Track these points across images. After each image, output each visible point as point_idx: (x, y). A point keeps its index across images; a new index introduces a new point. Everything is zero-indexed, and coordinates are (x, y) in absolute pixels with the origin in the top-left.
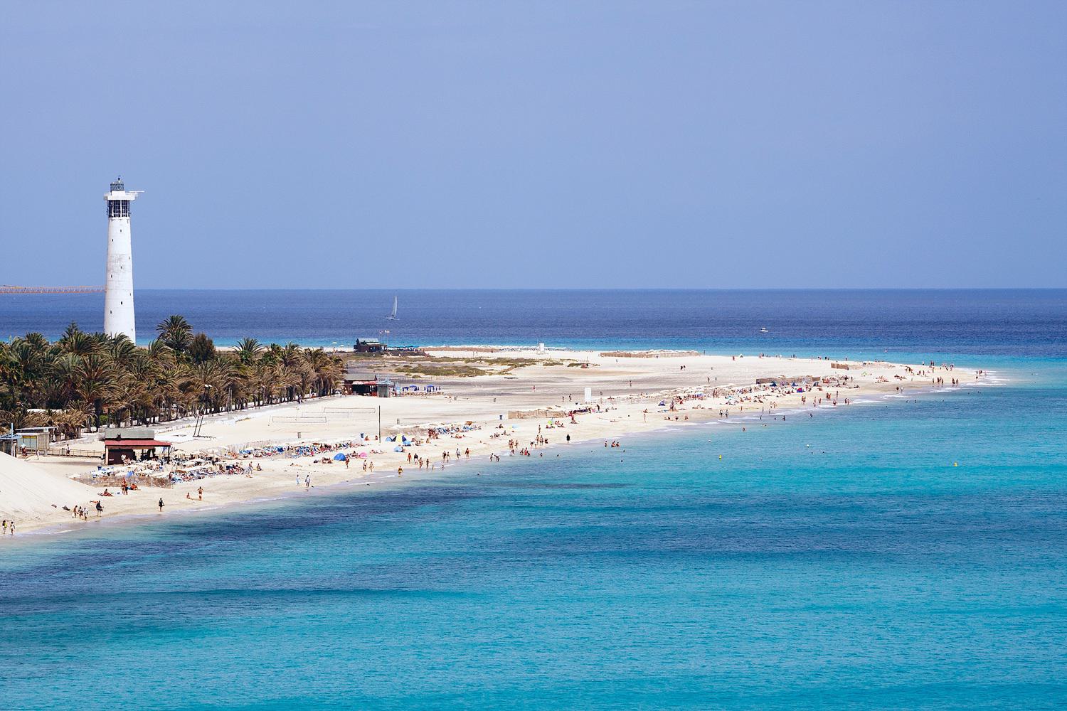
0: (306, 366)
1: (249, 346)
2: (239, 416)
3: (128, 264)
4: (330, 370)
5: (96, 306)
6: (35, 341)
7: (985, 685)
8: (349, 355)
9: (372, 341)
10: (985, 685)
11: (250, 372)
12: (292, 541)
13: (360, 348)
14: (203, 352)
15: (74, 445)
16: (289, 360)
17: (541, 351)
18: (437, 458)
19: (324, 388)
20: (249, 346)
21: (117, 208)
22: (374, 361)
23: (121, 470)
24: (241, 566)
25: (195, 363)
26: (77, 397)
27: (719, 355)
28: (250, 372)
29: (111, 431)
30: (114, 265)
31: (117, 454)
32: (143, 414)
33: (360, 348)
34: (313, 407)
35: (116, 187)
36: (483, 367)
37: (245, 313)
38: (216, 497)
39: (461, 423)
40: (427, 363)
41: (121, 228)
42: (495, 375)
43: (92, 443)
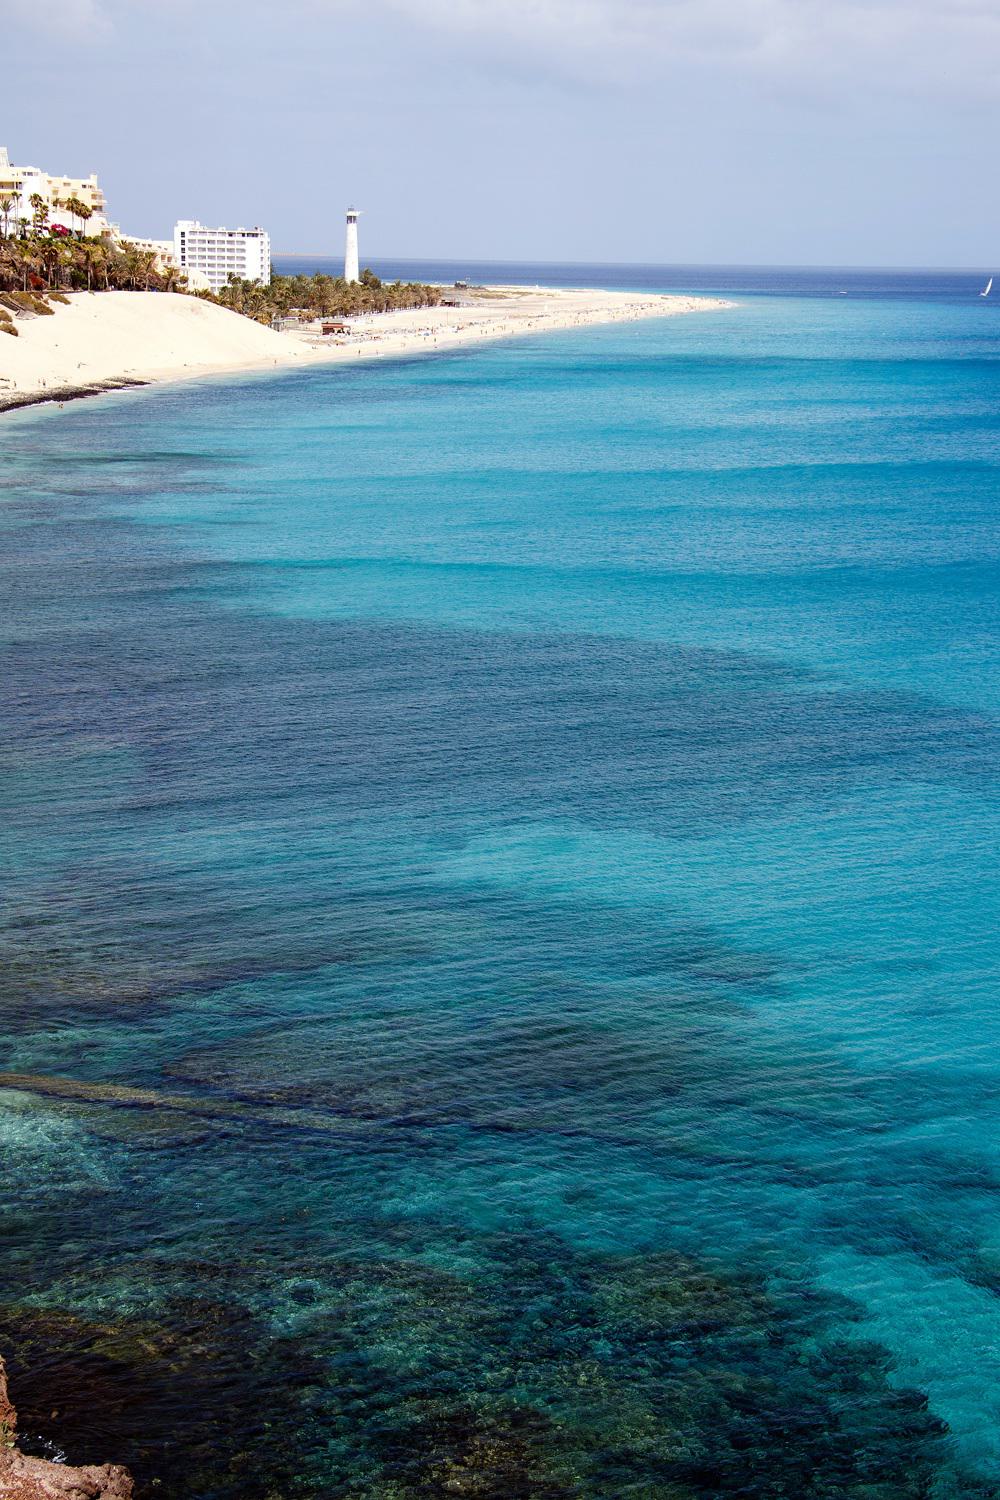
0: (423, 293)
1: (398, 285)
2: (391, 314)
3: (356, 244)
4: (434, 295)
5: (341, 267)
6: (299, 279)
7: (252, 1089)
8: (451, 289)
9: (463, 283)
10: (252, 1089)
11: (396, 295)
13: (457, 285)
14: (376, 285)
15: (310, 326)
16: (415, 290)
17: (536, 289)
19: (431, 303)
20: (398, 285)
21: (350, 219)
25: (379, 291)
27: (628, 291)
28: (396, 295)
29: (325, 320)
30: (349, 245)
31: (327, 330)
32: (345, 312)
33: (457, 285)
34: (425, 313)
35: (351, 210)
36: (510, 295)
38: (371, 350)
40: (485, 293)
41: (352, 228)
42: (512, 301)
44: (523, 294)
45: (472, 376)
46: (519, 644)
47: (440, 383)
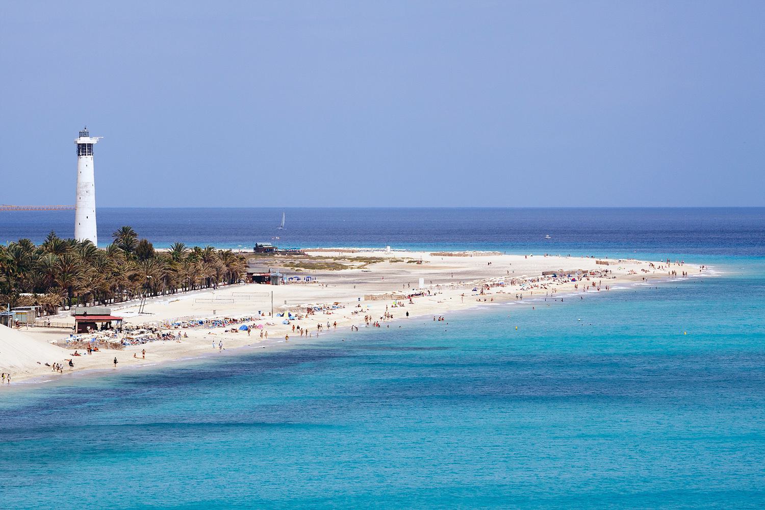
0: (220, 263)
1: (179, 248)
2: (172, 298)
3: (92, 189)
4: (237, 265)
5: (69, 219)
8: (250, 255)
9: (267, 244)
11: (179, 267)
13: (258, 250)
14: (145, 253)
15: (53, 319)
16: (208, 258)
17: (388, 252)
18: (313, 329)
19: (232, 279)
20: (179, 248)
21: (84, 149)
22: (268, 259)
23: (87, 337)
25: (140, 260)
26: (55, 285)
28: (179, 267)
29: (80, 309)
30: (82, 190)
31: (84, 326)
32: (103, 297)
33: (258, 250)
34: (225, 292)
35: (83, 134)
36: (347, 263)
38: (155, 357)
39: (331, 303)
40: (306, 261)
41: (87, 163)
42: (355, 269)
43: (66, 318)
44: (370, 261)
45: (429, 346)
46: (728, 279)
47: (401, 349)
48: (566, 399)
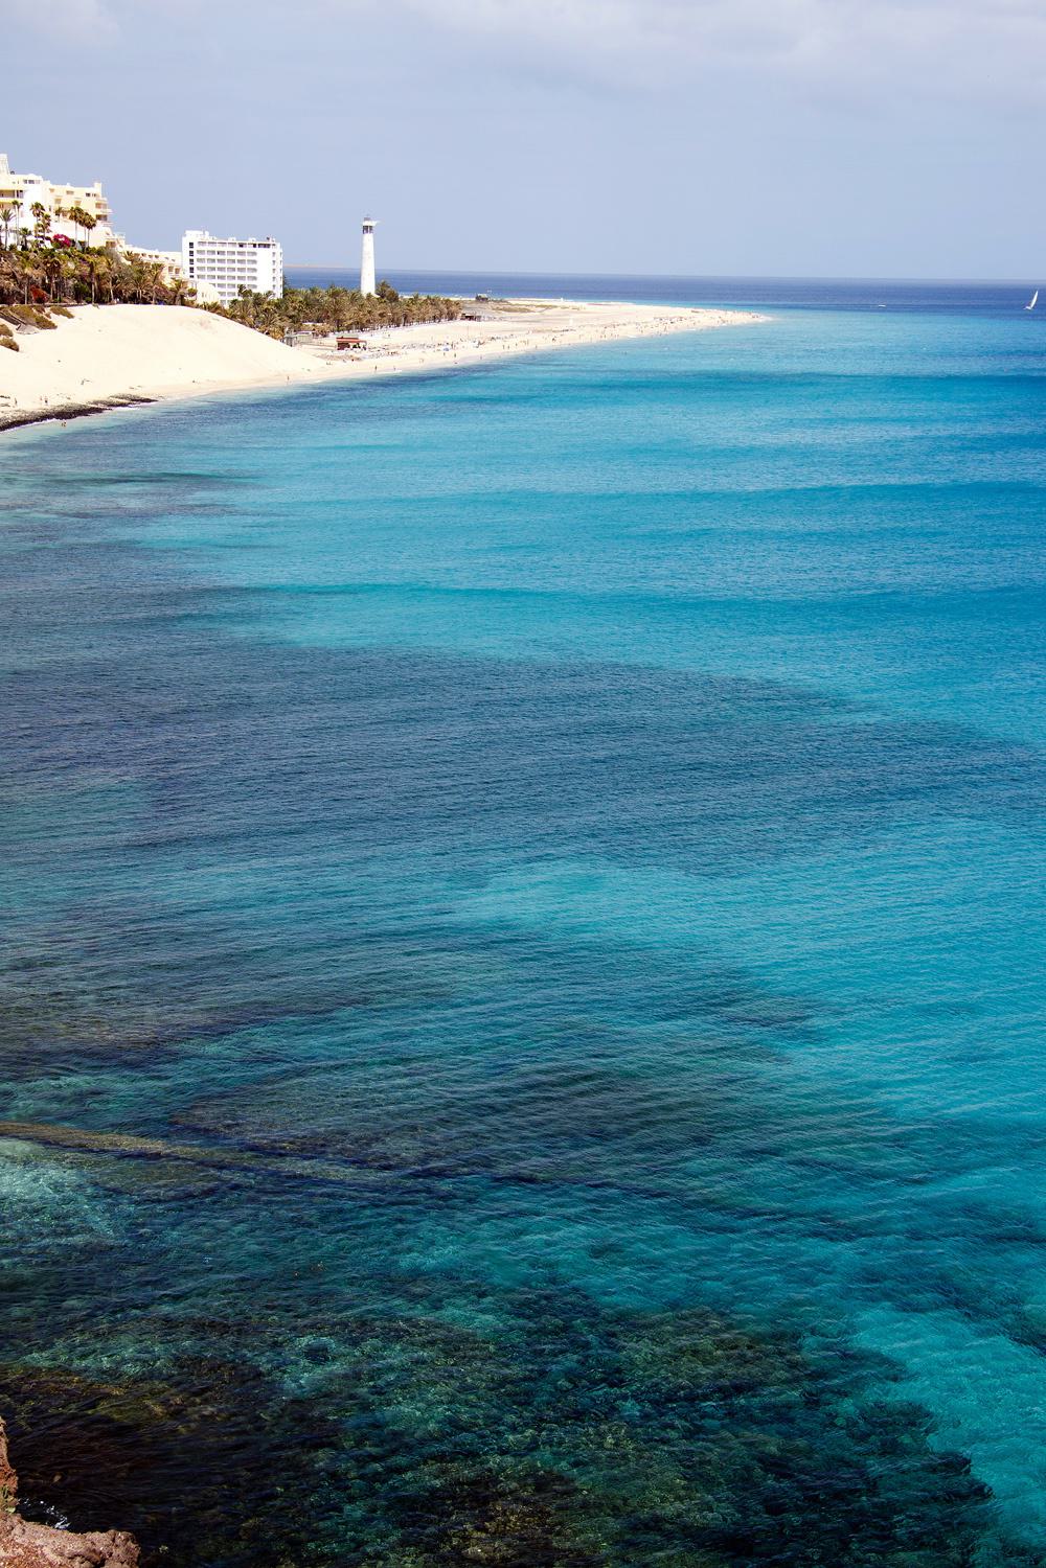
0: (442, 306)
1: (416, 297)
2: (406, 329)
3: (372, 255)
4: (453, 308)
5: (356, 280)
8: (472, 302)
9: (484, 296)
11: (414, 308)
12: (558, 411)
13: (478, 298)
14: (394, 298)
16: (434, 303)
17: (561, 302)
18: (492, 351)
20: (416, 297)
21: (366, 229)
22: (483, 305)
23: (342, 352)
24: (386, 399)
25: (396, 304)
26: (328, 317)
31: (342, 345)
32: (361, 327)
33: (478, 298)
35: (366, 219)
36: (533, 309)
37: (417, 282)
38: (388, 366)
39: (508, 335)
41: (368, 238)
42: (536, 315)
43: (332, 340)
44: (548, 307)
45: (495, 393)
48: (803, 308)
